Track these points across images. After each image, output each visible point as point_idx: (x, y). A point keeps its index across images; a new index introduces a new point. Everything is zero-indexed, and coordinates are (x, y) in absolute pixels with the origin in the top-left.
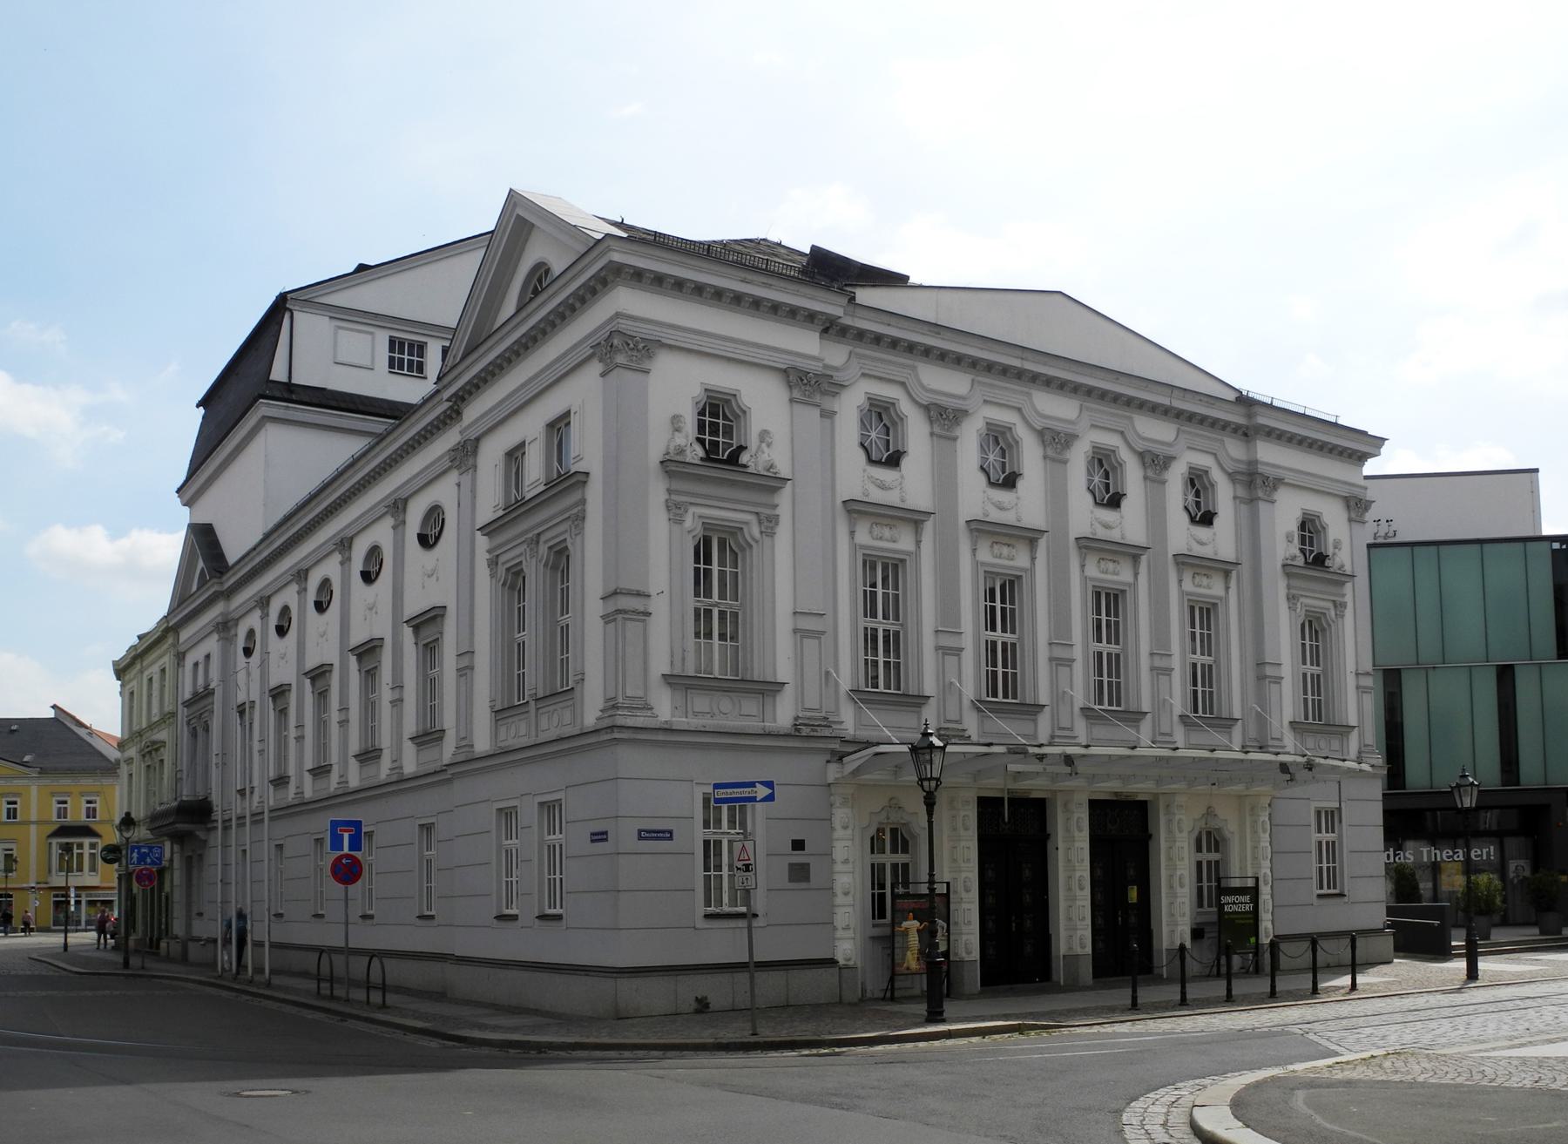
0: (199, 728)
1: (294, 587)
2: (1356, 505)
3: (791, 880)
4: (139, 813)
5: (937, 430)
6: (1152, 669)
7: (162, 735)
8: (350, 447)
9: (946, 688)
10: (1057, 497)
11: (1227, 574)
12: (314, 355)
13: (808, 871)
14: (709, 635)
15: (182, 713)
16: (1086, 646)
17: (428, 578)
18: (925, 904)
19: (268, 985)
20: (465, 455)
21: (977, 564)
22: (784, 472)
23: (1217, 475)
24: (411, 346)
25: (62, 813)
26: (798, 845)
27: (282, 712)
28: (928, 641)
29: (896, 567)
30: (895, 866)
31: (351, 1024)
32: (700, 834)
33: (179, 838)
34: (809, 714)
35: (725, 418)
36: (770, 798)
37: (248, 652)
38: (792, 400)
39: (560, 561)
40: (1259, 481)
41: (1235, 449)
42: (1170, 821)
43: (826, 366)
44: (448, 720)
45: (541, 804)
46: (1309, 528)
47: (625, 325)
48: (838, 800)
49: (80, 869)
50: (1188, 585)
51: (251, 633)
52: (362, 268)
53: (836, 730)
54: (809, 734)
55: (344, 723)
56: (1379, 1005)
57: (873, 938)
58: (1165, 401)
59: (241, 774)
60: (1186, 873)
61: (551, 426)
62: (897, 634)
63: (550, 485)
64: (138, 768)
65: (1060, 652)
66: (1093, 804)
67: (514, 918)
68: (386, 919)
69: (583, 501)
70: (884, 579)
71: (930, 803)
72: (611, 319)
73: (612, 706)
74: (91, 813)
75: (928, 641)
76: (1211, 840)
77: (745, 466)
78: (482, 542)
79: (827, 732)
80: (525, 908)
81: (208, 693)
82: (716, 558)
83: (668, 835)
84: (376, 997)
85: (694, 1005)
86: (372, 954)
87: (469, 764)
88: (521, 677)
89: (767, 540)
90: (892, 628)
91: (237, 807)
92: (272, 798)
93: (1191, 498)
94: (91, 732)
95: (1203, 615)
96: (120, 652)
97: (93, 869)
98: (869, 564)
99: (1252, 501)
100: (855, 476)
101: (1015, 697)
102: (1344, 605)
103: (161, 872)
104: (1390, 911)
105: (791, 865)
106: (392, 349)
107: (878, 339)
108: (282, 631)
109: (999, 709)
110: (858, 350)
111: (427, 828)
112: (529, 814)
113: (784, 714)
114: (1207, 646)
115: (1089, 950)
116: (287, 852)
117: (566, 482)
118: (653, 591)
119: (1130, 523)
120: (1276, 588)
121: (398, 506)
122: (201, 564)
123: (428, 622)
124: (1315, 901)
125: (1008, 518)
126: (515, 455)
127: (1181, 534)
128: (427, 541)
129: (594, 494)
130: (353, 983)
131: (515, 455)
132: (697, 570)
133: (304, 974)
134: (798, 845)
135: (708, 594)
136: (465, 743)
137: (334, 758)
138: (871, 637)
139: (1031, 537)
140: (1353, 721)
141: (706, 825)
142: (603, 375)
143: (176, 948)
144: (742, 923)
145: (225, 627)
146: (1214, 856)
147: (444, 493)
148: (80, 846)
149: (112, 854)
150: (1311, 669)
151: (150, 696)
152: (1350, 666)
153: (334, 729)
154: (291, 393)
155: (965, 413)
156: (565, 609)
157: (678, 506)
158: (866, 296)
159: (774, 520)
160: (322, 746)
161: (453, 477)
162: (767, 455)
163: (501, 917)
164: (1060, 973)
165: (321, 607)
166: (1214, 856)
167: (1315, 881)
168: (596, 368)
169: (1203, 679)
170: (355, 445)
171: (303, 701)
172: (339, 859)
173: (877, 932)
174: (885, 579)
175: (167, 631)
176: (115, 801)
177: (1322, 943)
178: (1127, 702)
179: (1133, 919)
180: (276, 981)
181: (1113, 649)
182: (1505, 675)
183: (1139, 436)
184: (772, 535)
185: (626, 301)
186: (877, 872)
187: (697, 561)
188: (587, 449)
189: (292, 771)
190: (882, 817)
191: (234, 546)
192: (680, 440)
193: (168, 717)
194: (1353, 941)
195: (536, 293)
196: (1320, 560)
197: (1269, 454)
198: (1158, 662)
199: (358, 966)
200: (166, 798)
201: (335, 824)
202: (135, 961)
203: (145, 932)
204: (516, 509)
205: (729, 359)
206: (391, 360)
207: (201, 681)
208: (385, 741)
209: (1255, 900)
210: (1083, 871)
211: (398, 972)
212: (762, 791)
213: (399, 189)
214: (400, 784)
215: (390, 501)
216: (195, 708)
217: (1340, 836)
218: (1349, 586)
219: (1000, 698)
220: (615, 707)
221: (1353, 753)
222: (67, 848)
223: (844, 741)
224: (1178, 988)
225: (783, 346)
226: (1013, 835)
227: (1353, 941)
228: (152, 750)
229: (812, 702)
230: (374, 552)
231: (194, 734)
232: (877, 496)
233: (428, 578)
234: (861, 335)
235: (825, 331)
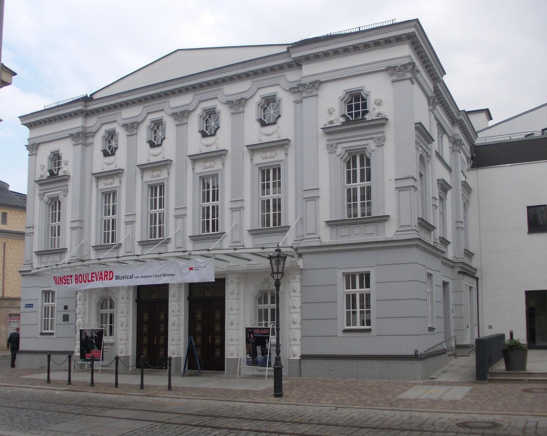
3: (64, 321)
13: (68, 317)
45: (43, 291)
69: (67, 186)
82: (358, 164)
98: (203, 179)
105: (64, 315)
110: (197, 93)
124: (340, 334)
129: (73, 186)
134: (66, 308)
141: (368, 295)
177: (53, 357)
192: (332, 118)
194: (49, 357)
210: (172, 319)
219: (211, 232)
226: (151, 302)
227: (49, 357)
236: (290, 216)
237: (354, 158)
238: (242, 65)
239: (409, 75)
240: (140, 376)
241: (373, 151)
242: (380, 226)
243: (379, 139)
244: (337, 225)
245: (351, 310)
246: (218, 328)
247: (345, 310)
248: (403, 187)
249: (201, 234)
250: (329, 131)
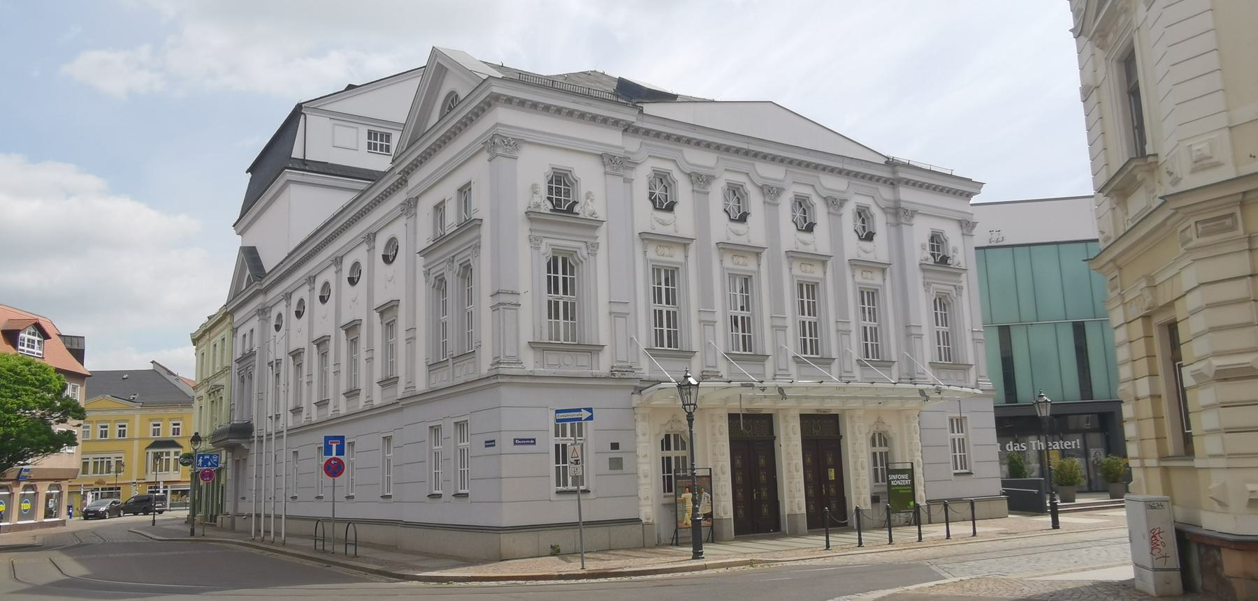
0: (245, 376)
1: (307, 287)
2: (967, 226)
4: (205, 432)
5: (696, 188)
6: (838, 331)
7: (222, 381)
8: (345, 198)
9: (707, 346)
10: (772, 227)
11: (884, 270)
12: (317, 141)
14: (557, 317)
15: (235, 366)
16: (794, 318)
17: (389, 282)
18: (689, 482)
19: (284, 544)
20: (410, 206)
22: (601, 216)
23: (875, 210)
24: (382, 135)
25: (156, 432)
26: (615, 446)
27: (324, 355)
29: (673, 272)
30: (677, 458)
31: (334, 568)
32: (553, 441)
33: (231, 448)
36: (591, 418)
37: (278, 328)
38: (605, 173)
39: (467, 271)
40: (902, 213)
41: (886, 193)
44: (401, 371)
46: (936, 240)
47: (501, 131)
48: (639, 417)
49: (167, 469)
50: (859, 278)
51: (280, 316)
52: (350, 87)
53: (638, 374)
54: (620, 377)
55: (370, 360)
56: (988, 545)
57: (664, 505)
58: (840, 166)
59: (272, 408)
60: (865, 460)
61: (460, 190)
62: (675, 313)
63: (460, 226)
64: (206, 402)
65: (778, 322)
66: (804, 418)
67: (439, 496)
68: (360, 497)
69: (479, 237)
70: (666, 283)
71: (690, 419)
72: (494, 127)
73: (497, 363)
74: (176, 432)
76: (880, 439)
78: (420, 260)
79: (631, 375)
80: (446, 491)
81: (252, 354)
83: (532, 442)
84: (351, 550)
85: (550, 550)
86: (349, 522)
87: (414, 400)
88: (444, 344)
89: (592, 258)
90: (671, 310)
91: (270, 427)
92: (289, 421)
93: (859, 223)
94: (178, 379)
95: (869, 297)
96: (196, 328)
97: (176, 469)
98: (656, 270)
99: (898, 225)
100: (646, 218)
102: (961, 288)
103: (219, 471)
104: (1004, 484)
106: (369, 138)
107: (658, 135)
108: (299, 314)
109: (738, 358)
110: (648, 142)
111: (387, 439)
112: (448, 429)
113: (604, 365)
114: (873, 315)
115: (804, 510)
116: (394, 443)
117: (469, 225)
118: (522, 292)
119: (819, 241)
120: (916, 279)
121: (370, 238)
122: (248, 272)
123: (388, 310)
124: (554, 497)
125: (742, 240)
126: (439, 208)
127: (852, 247)
128: (387, 259)
129: (486, 231)
130: (336, 541)
131: (439, 208)
132: (549, 278)
133: (308, 536)
135: (556, 291)
136: (410, 385)
137: (331, 395)
139: (757, 252)
140: (971, 361)
142: (490, 160)
143: (227, 521)
144: (575, 497)
145: (263, 312)
146: (884, 449)
147: (398, 230)
148: (168, 454)
149: (187, 459)
150: (942, 329)
151: (214, 355)
152: (968, 326)
153: (331, 376)
154: (305, 165)
155: (713, 177)
156: (470, 303)
158: (650, 108)
159: (596, 246)
160: (323, 387)
161: (403, 220)
162: (591, 207)
163: (432, 496)
164: (785, 525)
165: (323, 299)
166: (884, 449)
167: (952, 465)
168: (485, 156)
169: (871, 337)
170: (347, 197)
171: (311, 359)
172: (329, 461)
173: (667, 501)
174: (667, 280)
175: (226, 314)
176: (197, 421)
177: (952, 506)
179: (832, 491)
180: (289, 541)
181: (812, 319)
182: (1079, 330)
185: (503, 116)
186: (667, 462)
187: (549, 272)
188: (481, 205)
189: (304, 404)
190: (668, 427)
191: (269, 262)
192: (537, 199)
193: (225, 370)
194: (946, 506)
195: (451, 109)
196: (944, 260)
197: (908, 196)
198: (841, 327)
199: (340, 529)
200: (223, 422)
201: (327, 439)
202: (198, 531)
203: (206, 511)
204: (440, 241)
205: (567, 149)
206: (369, 144)
207: (247, 347)
208: (362, 384)
209: (912, 478)
211: (364, 532)
212: (585, 414)
213: (357, 57)
214: (372, 412)
215: (365, 234)
216: (244, 363)
217: (967, 436)
218: (964, 275)
219: (666, 347)
220: (498, 363)
221: (973, 383)
222: (157, 457)
223: (642, 380)
226: (752, 437)
227: (946, 506)
228: (215, 391)
230: (356, 266)
231: (242, 380)
232: (660, 229)
233: (389, 282)
234: (647, 132)
235: (626, 130)
246: (739, 479)
247: (553, 465)
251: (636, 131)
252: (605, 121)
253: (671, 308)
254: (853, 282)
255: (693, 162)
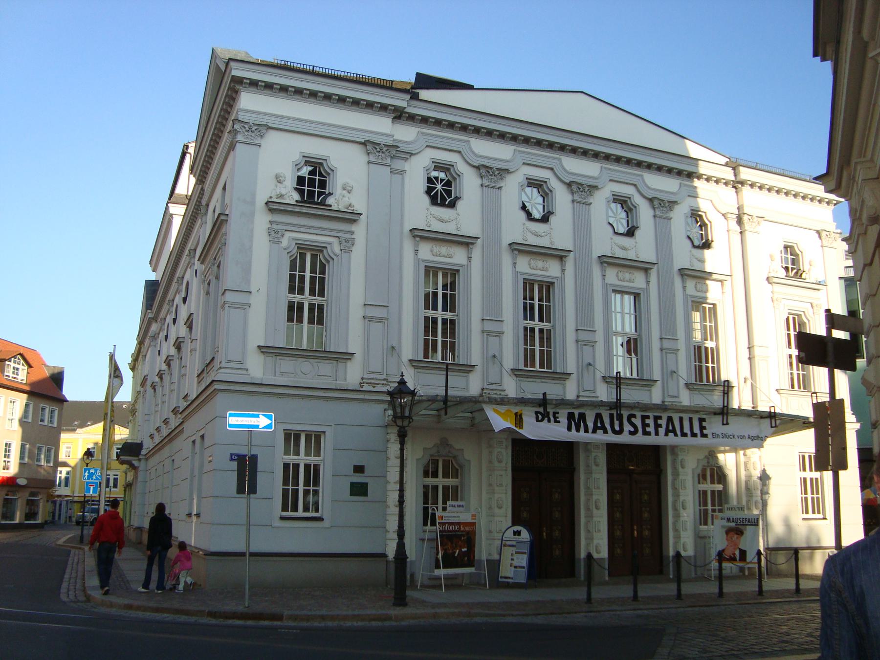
3: (351, 494)
14: (300, 320)
21: (516, 274)
22: (359, 207)
26: (359, 469)
28: (656, 345)
34: (372, 376)
35: (321, 175)
42: (674, 462)
43: (395, 140)
62: (549, 331)
75: (656, 345)
77: (330, 206)
89: (345, 255)
98: (528, 284)
100: (419, 211)
101: (549, 367)
105: (352, 484)
118: (253, 289)
138: (430, 325)
157: (276, 232)
159: (351, 242)
178: (643, 374)
183: (473, 152)
184: (349, 251)
205: (618, 182)
219: (537, 368)
224: (585, 589)
225: (284, 114)
229: (376, 366)
234: (425, 120)
236: (568, 357)
237: (303, 256)
238: (786, 173)
239: (388, 161)
240: (632, 587)
241: (337, 256)
242: (341, 365)
243: (347, 241)
244: (277, 354)
245: (311, 488)
248: (376, 318)
249: (522, 367)
250: (273, 207)
251: (412, 118)
252: (370, 105)
253: (449, 315)
254: (511, 274)
255: (573, 171)
